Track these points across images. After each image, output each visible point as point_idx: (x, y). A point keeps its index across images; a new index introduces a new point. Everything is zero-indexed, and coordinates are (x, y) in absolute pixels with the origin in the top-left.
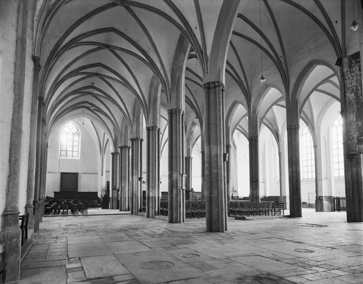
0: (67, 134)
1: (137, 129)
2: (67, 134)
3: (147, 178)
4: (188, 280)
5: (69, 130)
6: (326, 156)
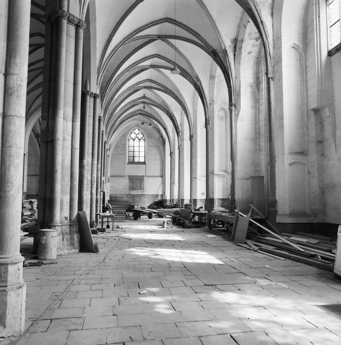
0: (134, 140)
1: (226, 127)
2: (134, 140)
3: (274, 152)
4: (69, 276)
5: (136, 136)
6: (226, 140)
